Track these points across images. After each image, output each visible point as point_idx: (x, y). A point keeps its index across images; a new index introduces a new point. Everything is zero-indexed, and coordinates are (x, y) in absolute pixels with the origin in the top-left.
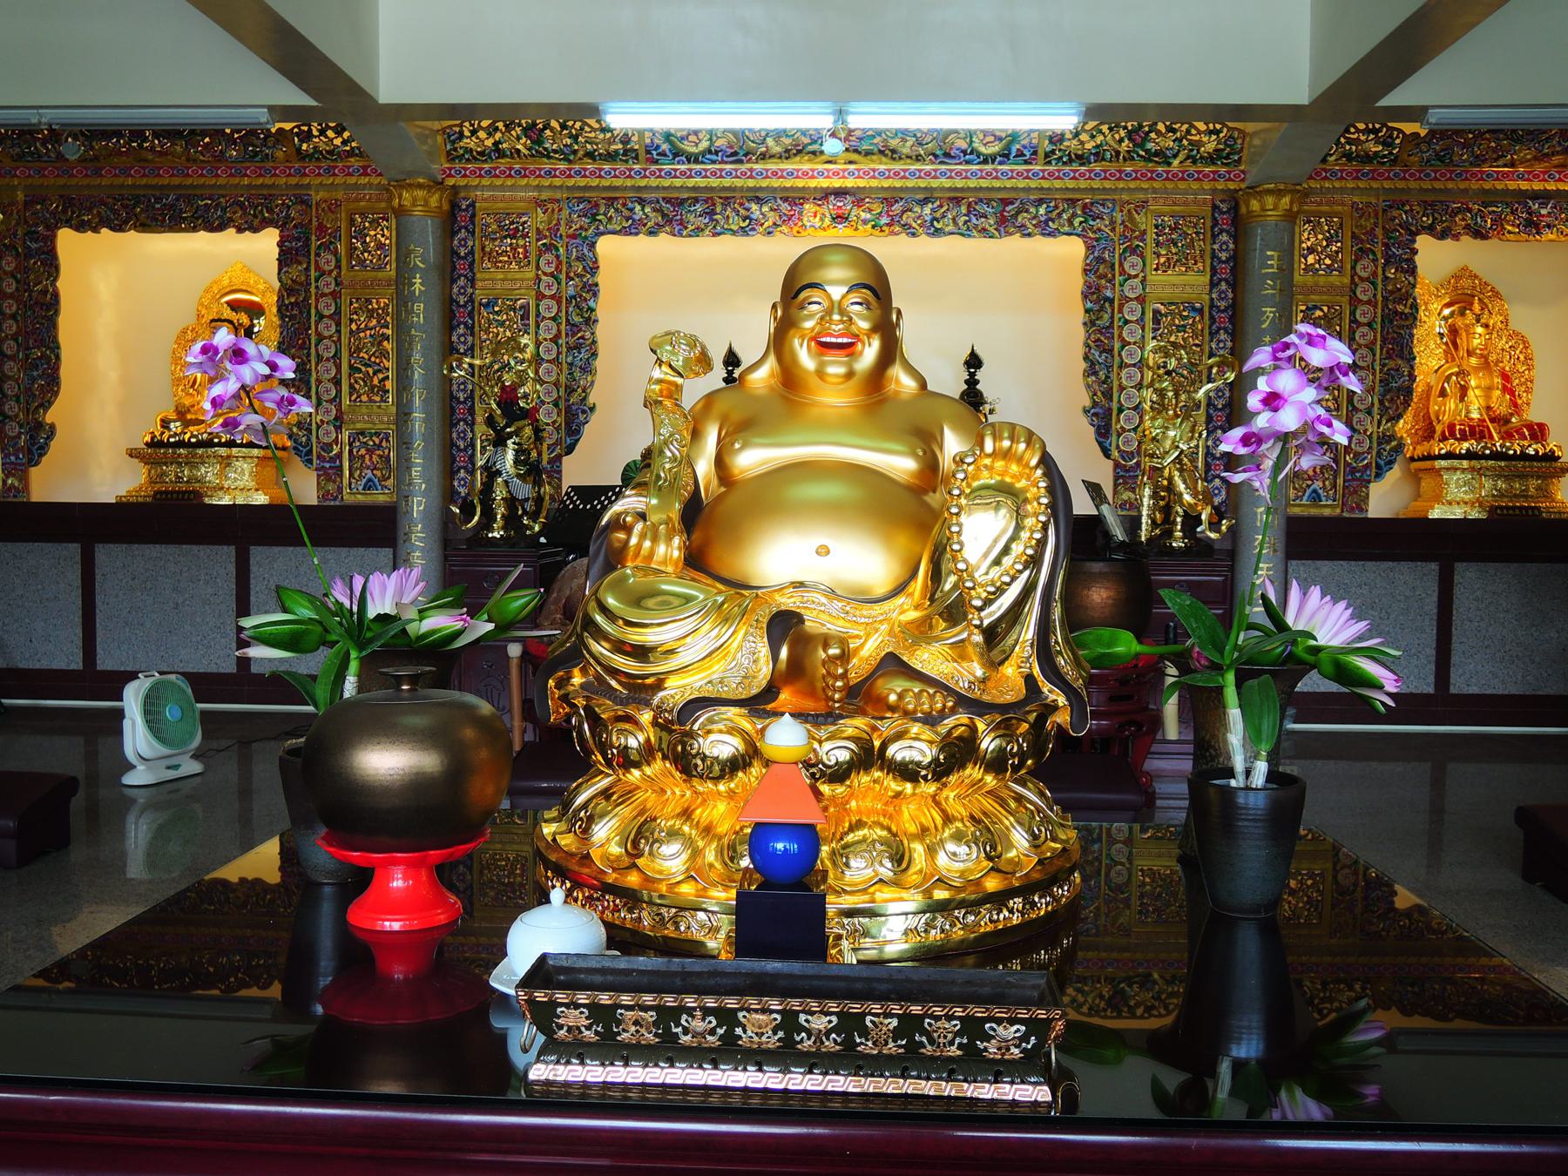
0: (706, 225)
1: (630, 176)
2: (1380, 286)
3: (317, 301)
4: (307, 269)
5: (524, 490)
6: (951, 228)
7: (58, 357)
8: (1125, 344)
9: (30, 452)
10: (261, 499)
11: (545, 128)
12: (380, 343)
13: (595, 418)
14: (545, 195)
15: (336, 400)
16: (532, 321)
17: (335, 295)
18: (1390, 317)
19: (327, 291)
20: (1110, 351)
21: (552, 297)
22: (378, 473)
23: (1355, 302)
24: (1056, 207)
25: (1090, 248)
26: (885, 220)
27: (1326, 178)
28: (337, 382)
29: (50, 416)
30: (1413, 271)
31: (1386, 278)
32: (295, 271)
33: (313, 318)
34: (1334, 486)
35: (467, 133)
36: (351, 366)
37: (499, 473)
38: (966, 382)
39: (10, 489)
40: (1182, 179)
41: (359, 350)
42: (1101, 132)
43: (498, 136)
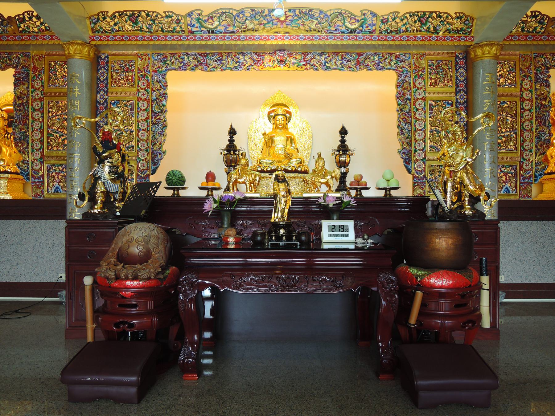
0: (218, 65)
1: (180, 40)
2: (534, 93)
3: (32, 102)
4: (28, 87)
5: (115, 188)
6: (334, 66)
8: (417, 120)
10: (8, 197)
11: (139, 16)
12: (63, 122)
13: (166, 157)
14: (142, 52)
15: (41, 149)
16: (135, 111)
17: (41, 99)
18: (540, 107)
19: (37, 97)
20: (410, 123)
21: (145, 100)
22: (61, 184)
23: (522, 99)
24: (383, 57)
25: (399, 75)
26: (303, 63)
27: (511, 40)
28: (41, 141)
30: (548, 86)
31: (536, 89)
32: (22, 88)
33: (30, 111)
34: (516, 186)
35: (101, 19)
36: (48, 133)
37: (99, 178)
38: (340, 141)
40: (444, 40)
41: (53, 125)
42: (406, 17)
43: (116, 20)
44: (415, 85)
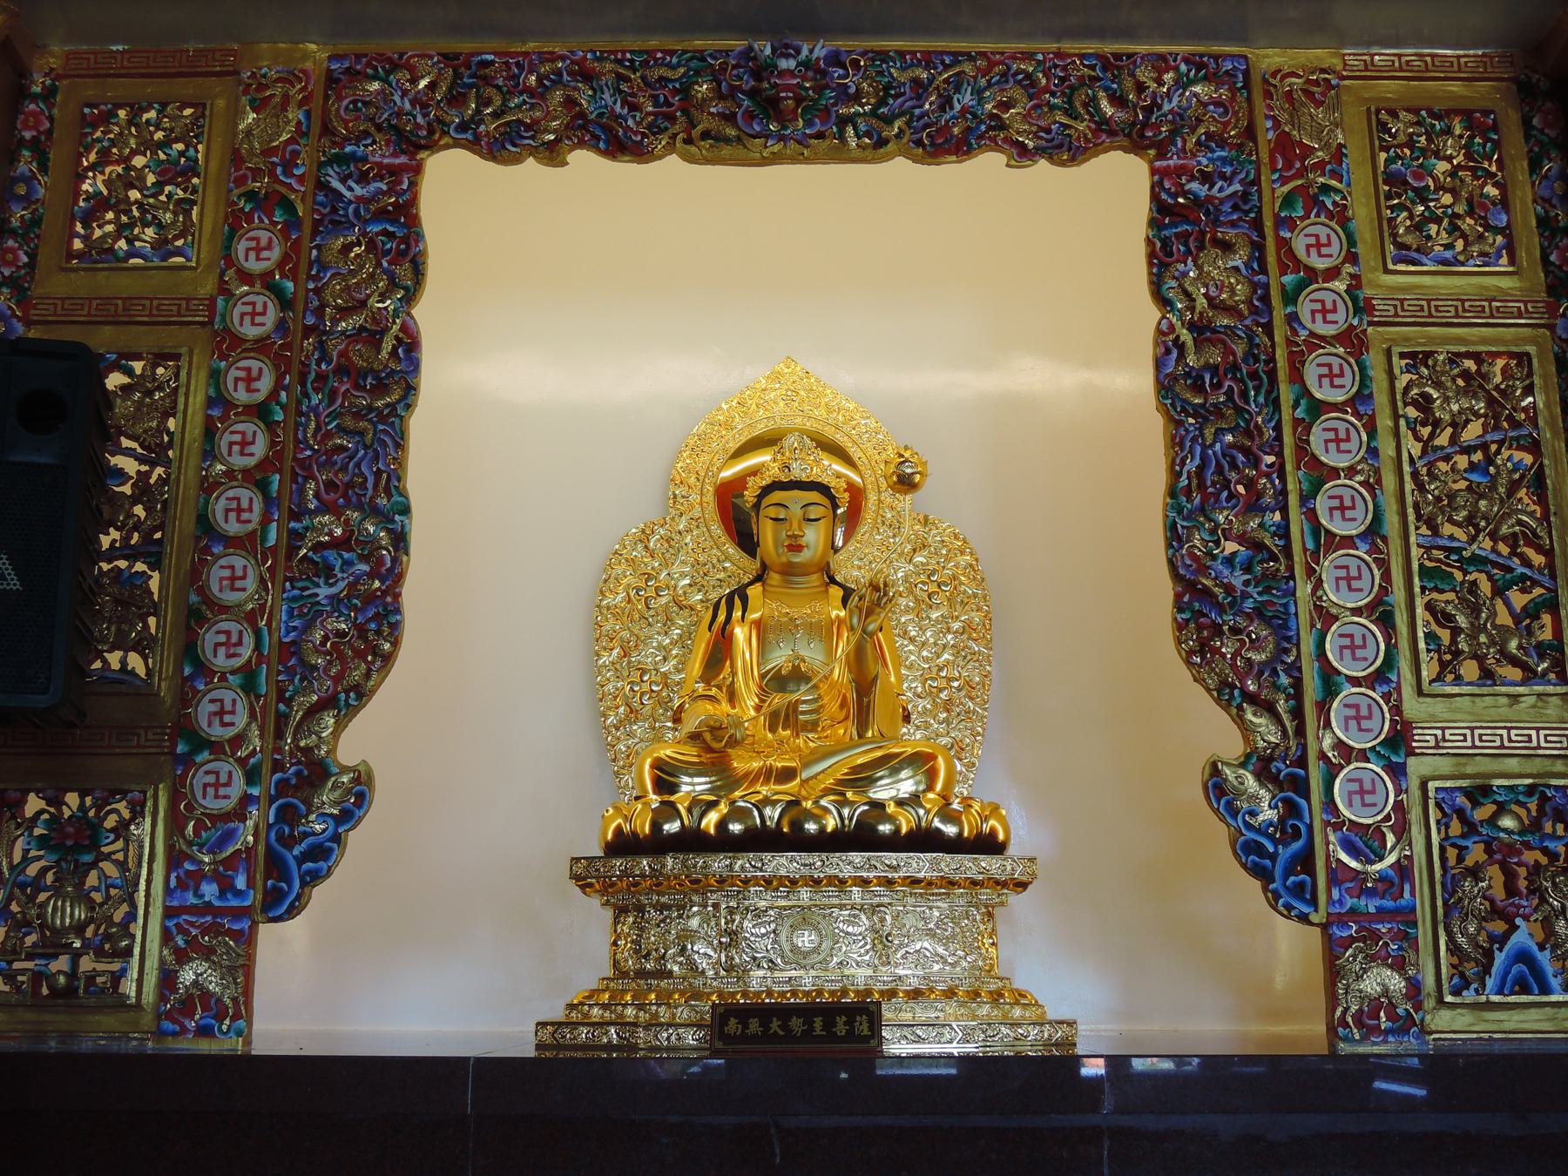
7: (400, 540)
9: (275, 866)
29: (356, 742)
32: (1219, 274)
39: (187, 1006)
44: (1291, 253)
